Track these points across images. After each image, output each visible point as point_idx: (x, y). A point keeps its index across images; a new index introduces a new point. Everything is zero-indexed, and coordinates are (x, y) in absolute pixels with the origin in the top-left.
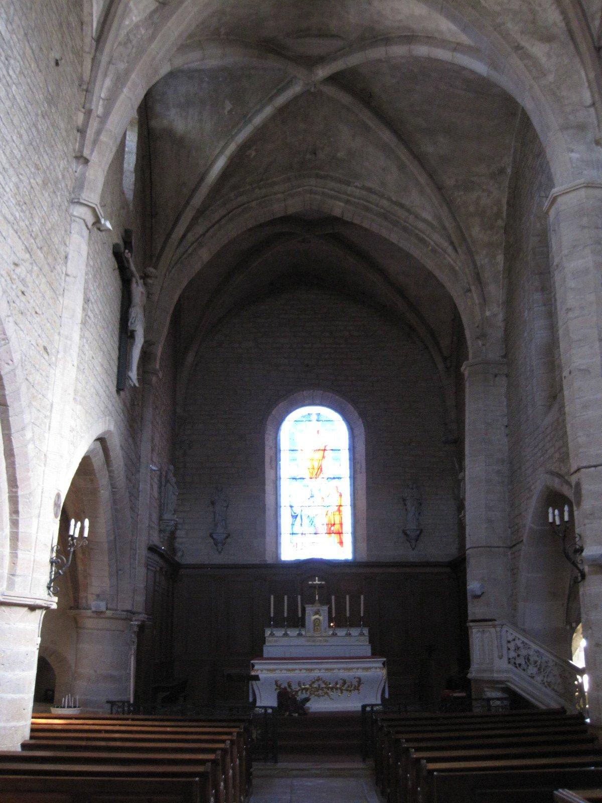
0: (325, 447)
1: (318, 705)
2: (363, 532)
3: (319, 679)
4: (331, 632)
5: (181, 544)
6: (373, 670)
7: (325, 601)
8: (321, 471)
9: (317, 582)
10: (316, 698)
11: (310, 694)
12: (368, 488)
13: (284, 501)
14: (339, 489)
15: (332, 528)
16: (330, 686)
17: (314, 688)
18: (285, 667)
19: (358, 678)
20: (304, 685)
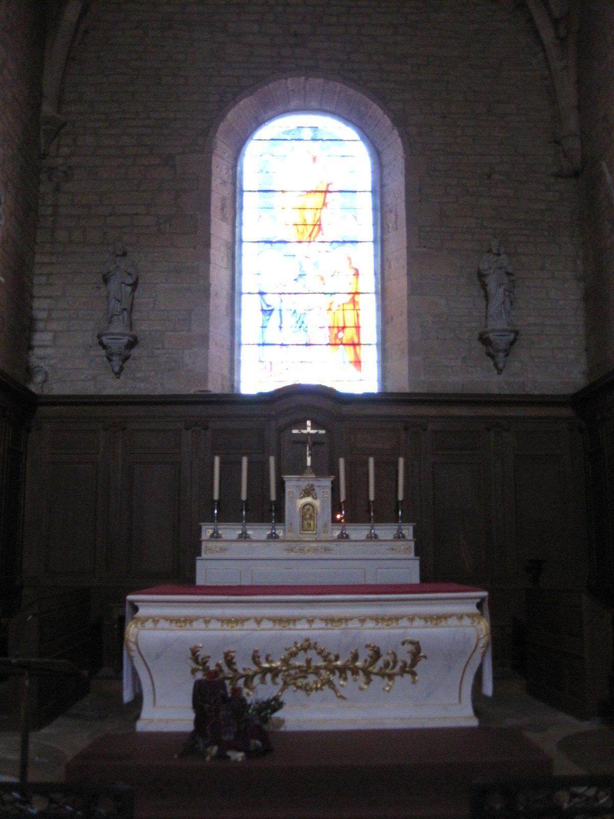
0: (328, 185)
1: (306, 713)
2: (400, 336)
3: (307, 646)
4: (337, 533)
5: (42, 358)
6: (453, 622)
7: (325, 468)
8: (320, 229)
9: (309, 430)
10: (301, 694)
12: (412, 257)
13: (248, 282)
14: (353, 261)
15: (340, 335)
16: (339, 663)
18: (217, 611)
19: (412, 643)
20: (268, 661)
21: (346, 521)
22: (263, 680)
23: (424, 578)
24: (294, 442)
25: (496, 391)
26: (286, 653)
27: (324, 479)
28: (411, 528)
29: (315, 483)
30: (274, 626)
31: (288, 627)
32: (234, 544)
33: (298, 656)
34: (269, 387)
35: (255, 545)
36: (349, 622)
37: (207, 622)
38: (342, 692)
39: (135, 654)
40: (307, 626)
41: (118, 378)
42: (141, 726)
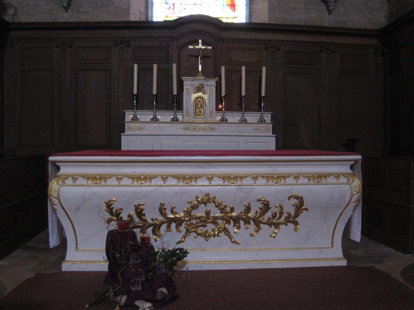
1: (206, 255)
4: (219, 118)
6: (331, 180)
7: (212, 72)
10: (201, 239)
11: (188, 231)
16: (233, 214)
17: (196, 218)
19: (297, 197)
20: (172, 212)
21: (226, 110)
22: (169, 227)
23: (277, 148)
24: (190, 56)
25: (327, 25)
26: (189, 206)
27: (211, 80)
28: (270, 115)
29: (205, 83)
30: (178, 182)
31: (190, 184)
32: (147, 125)
33: (198, 208)
34: (172, 17)
35: (162, 125)
36: (243, 180)
37: (119, 179)
38: (236, 238)
39: (58, 207)
40: (207, 183)
41: (67, 11)
42: (66, 267)
